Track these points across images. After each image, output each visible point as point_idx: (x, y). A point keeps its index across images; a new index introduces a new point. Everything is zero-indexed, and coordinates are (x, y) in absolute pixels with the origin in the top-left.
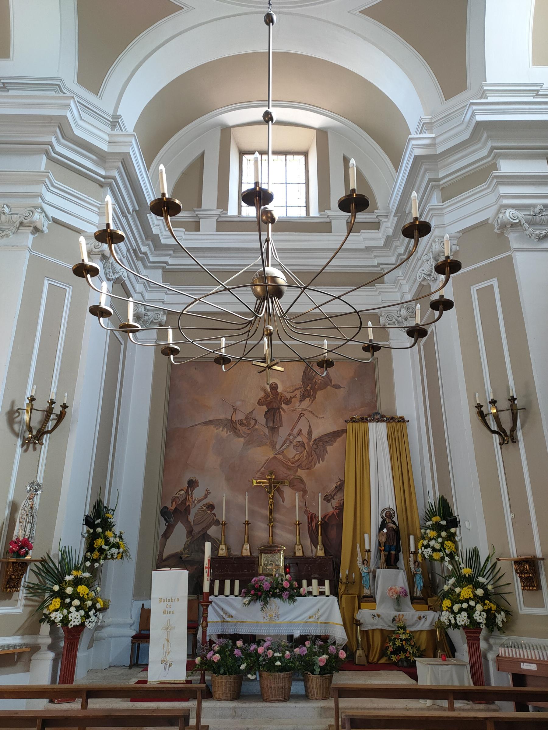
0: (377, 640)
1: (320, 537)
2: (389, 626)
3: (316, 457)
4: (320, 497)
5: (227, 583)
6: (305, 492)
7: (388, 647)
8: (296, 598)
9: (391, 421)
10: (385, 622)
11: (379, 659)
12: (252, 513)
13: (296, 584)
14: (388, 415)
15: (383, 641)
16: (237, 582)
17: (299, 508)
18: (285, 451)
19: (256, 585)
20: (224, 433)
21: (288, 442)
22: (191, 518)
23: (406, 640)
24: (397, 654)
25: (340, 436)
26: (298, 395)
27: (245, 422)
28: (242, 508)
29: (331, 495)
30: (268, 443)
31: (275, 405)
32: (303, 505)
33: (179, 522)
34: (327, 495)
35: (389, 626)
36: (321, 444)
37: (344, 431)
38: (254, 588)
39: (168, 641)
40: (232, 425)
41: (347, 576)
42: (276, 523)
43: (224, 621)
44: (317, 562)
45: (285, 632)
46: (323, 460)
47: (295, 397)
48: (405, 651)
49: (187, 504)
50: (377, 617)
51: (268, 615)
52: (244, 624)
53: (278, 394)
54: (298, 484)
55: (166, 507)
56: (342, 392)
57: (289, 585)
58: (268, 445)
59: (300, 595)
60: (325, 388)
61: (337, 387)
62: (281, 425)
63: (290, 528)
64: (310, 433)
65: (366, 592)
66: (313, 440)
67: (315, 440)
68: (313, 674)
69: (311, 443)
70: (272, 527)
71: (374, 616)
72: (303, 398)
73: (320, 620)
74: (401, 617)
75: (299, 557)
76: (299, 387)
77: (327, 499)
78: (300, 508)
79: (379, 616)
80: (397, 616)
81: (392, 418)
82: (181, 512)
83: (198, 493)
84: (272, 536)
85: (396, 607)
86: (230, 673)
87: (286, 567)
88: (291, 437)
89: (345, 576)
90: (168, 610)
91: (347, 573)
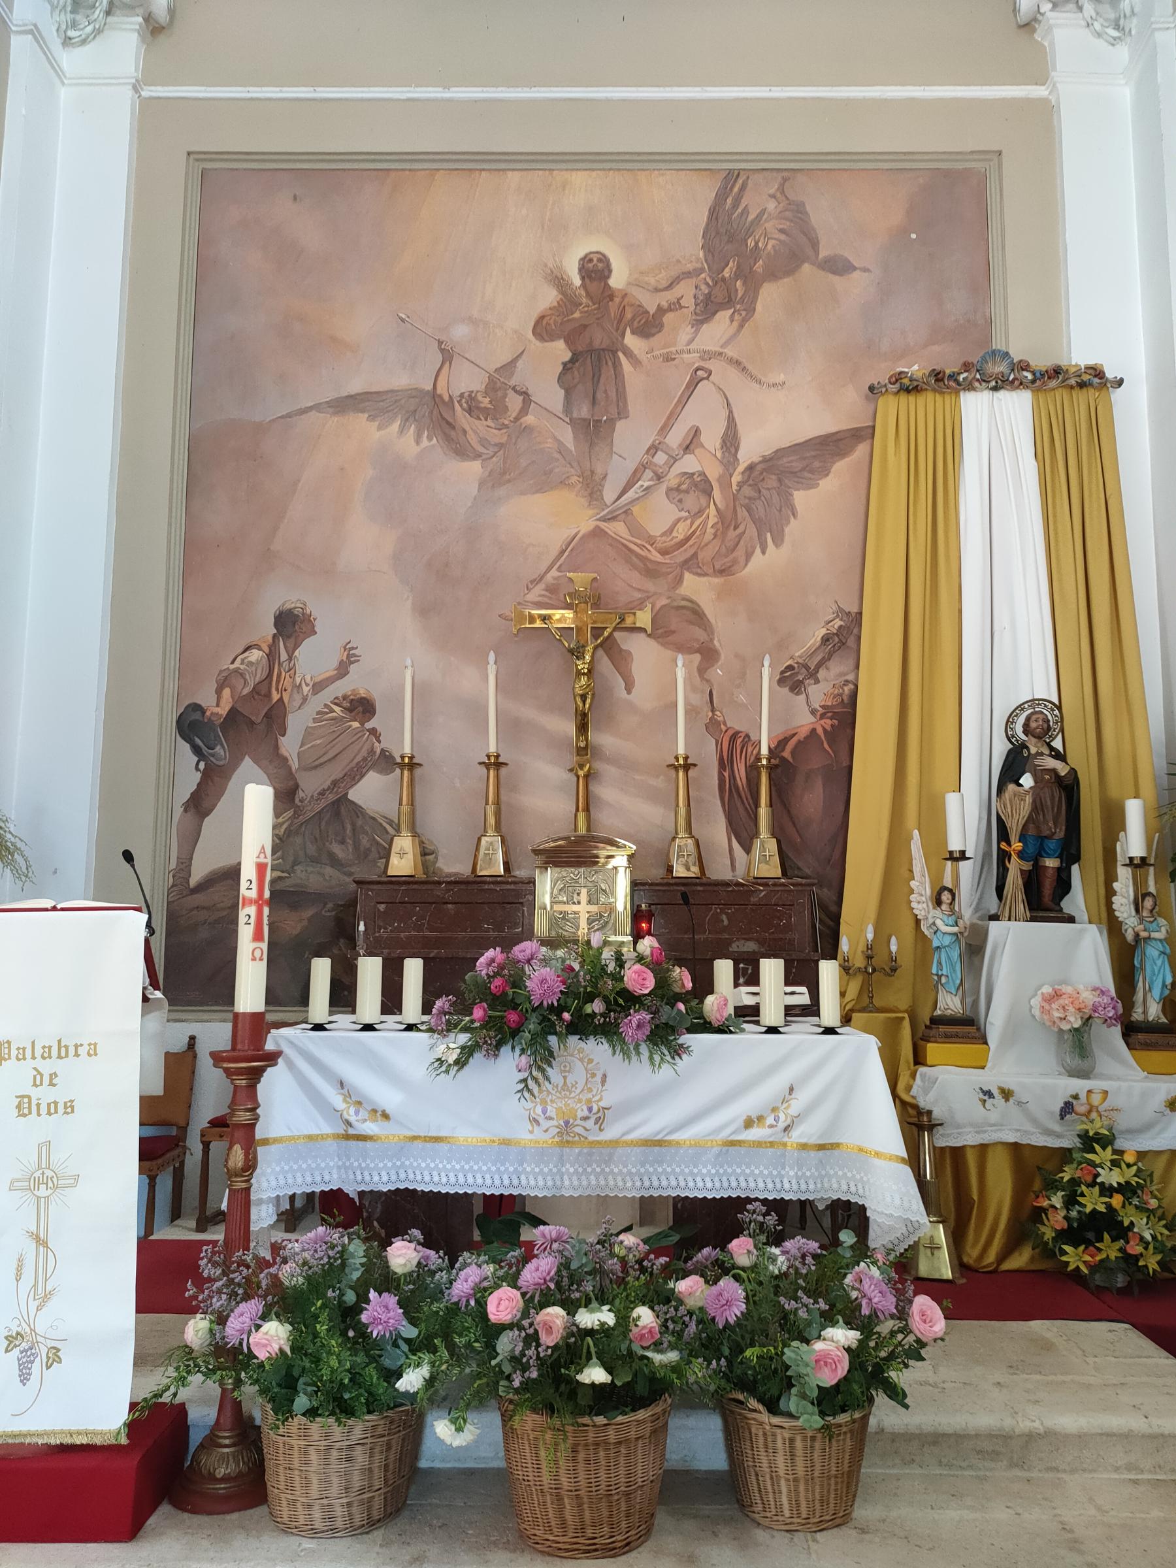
0: (999, 1190)
1: (763, 811)
2: (1049, 1132)
3: (752, 531)
4: (766, 672)
5: (370, 971)
6: (708, 655)
7: (1044, 1210)
8: (687, 1039)
9: (1053, 383)
10: (1034, 1121)
11: (1004, 1255)
12: (511, 727)
13: (682, 978)
14: (1041, 363)
15: (1022, 1189)
16: (413, 969)
17: (687, 712)
18: (636, 510)
19: (498, 981)
20: (406, 442)
21: (649, 474)
22: (290, 745)
23: (1126, 1190)
24: (1088, 1243)
25: (842, 454)
26: (688, 301)
27: (485, 402)
28: (477, 711)
29: (806, 667)
30: (574, 479)
31: (599, 339)
32: (700, 700)
33: (247, 759)
34: (790, 668)
35: (1049, 1132)
36: (772, 481)
37: (864, 434)
38: (484, 993)
39: (41, 1241)
40: (436, 413)
41: (870, 947)
42: (599, 765)
43: (347, 1137)
44: (753, 900)
45: (630, 1180)
46: (778, 541)
47: (676, 306)
48: (1122, 1232)
49: (275, 696)
50: (999, 1100)
51: (551, 1111)
52: (444, 1147)
53: (611, 297)
54: (684, 629)
55: (196, 707)
56: (856, 288)
57: (651, 983)
58: (571, 486)
59: (706, 1027)
60: (789, 272)
61: (838, 267)
62: (623, 413)
63: (653, 782)
64: (731, 441)
65: (950, 1003)
66: (741, 468)
67: (751, 468)
68: (773, 1408)
69: (736, 478)
70: (587, 776)
71: (989, 1094)
72: (707, 309)
73: (798, 1135)
74: (1096, 1099)
75: (684, 882)
76: (690, 267)
77: (793, 679)
78: (691, 711)
79: (1007, 1094)
80: (1083, 1096)
81: (1057, 371)
82: (253, 723)
83: (313, 658)
84: (587, 809)
85: (1073, 1061)
86: (343, 1409)
87: (637, 916)
88: (660, 458)
89: (862, 947)
90: (45, 1094)
91: (870, 936)
